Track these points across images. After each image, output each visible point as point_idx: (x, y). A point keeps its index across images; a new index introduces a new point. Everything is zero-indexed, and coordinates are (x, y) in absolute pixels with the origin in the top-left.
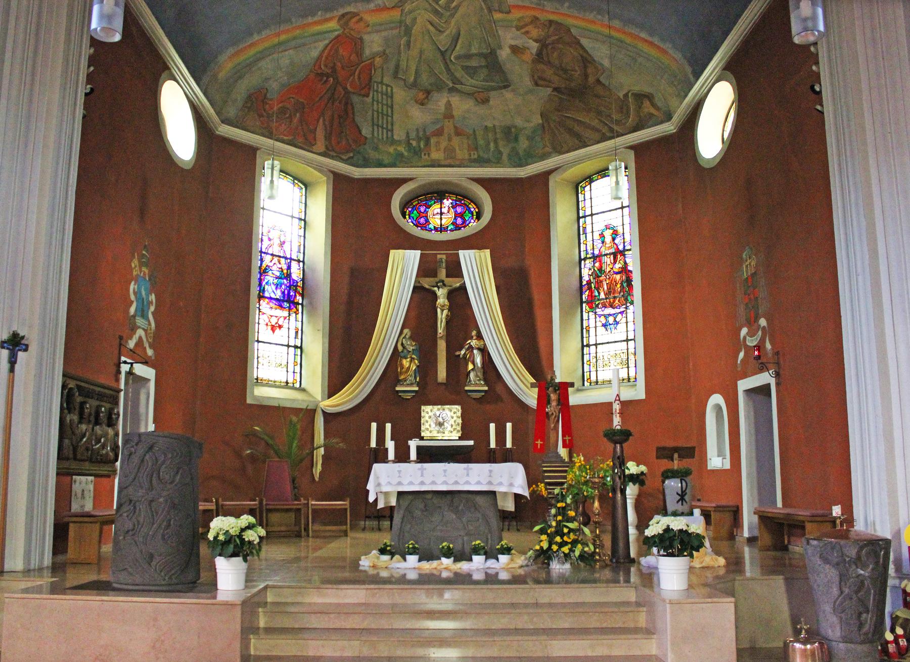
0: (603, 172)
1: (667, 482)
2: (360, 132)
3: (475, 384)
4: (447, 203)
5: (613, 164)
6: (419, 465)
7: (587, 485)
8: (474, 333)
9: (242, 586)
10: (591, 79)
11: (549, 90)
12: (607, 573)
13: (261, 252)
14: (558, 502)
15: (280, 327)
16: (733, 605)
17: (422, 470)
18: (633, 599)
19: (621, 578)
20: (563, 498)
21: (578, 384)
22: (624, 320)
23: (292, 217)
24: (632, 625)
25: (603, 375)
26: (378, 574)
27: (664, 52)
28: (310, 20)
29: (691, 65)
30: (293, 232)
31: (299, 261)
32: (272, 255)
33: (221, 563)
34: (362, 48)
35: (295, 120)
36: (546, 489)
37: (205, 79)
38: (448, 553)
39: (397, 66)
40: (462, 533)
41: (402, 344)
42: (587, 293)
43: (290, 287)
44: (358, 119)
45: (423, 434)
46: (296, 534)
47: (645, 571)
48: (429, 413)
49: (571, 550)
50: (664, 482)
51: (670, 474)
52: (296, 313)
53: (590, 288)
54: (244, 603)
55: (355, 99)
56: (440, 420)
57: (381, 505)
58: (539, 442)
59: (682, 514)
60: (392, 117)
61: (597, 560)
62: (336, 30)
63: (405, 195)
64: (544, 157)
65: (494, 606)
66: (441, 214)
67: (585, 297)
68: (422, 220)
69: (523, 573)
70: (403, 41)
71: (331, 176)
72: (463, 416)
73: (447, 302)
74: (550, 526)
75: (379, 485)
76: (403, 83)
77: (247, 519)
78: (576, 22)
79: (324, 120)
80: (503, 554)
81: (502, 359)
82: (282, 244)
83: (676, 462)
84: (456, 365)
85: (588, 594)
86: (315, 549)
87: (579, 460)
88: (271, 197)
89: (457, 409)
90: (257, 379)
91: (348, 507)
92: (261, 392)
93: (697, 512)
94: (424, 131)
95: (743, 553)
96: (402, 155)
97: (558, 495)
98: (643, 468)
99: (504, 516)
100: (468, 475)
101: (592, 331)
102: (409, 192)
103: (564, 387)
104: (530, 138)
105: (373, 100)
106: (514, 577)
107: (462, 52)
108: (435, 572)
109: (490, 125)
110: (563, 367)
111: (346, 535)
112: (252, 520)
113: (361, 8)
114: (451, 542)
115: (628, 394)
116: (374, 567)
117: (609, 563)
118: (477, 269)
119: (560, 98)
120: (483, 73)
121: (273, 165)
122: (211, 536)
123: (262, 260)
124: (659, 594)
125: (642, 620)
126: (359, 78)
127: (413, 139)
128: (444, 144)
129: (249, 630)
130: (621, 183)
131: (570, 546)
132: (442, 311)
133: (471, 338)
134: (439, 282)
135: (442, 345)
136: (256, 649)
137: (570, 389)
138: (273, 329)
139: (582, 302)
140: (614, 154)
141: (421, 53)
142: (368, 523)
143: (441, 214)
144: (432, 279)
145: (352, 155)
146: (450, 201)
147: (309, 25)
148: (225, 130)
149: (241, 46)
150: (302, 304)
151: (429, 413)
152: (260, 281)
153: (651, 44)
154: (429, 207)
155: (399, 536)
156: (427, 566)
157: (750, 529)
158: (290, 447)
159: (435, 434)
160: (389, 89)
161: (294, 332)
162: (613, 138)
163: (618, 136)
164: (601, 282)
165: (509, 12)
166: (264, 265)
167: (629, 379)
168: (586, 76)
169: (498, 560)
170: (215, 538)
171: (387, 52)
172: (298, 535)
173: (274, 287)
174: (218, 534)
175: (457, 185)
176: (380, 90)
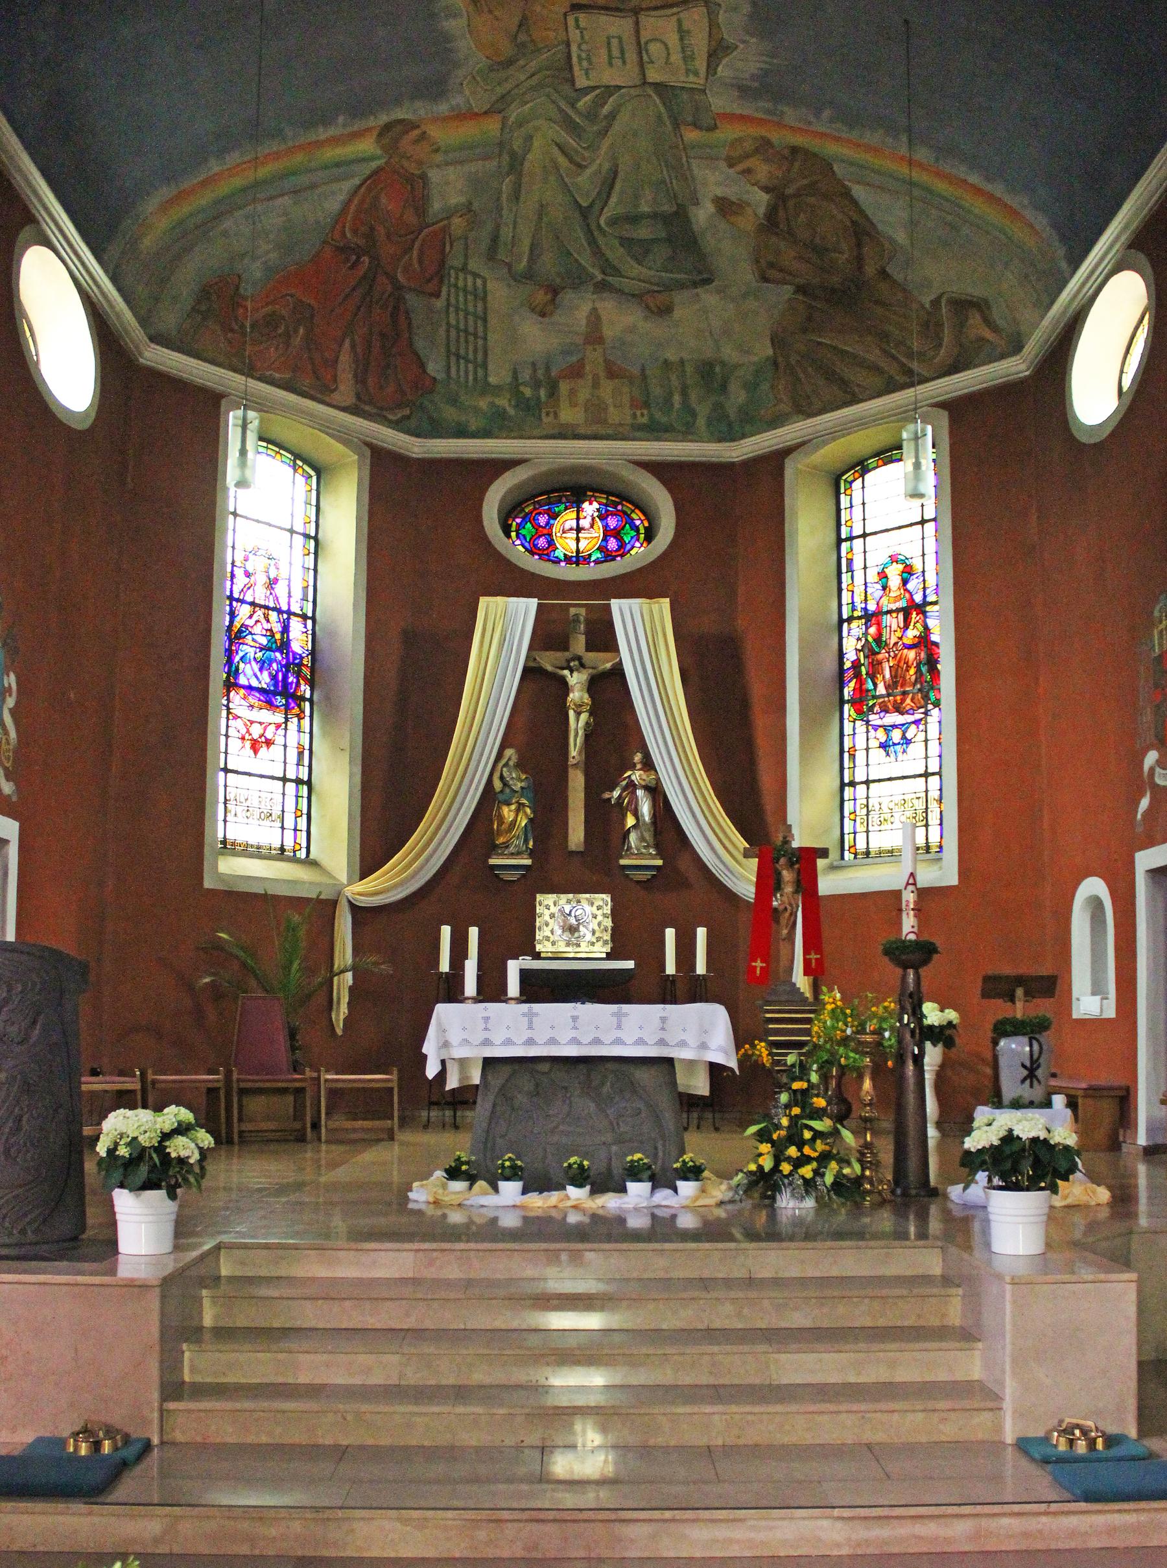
0: (889, 453)
1: (1002, 1043)
2: (422, 366)
3: (639, 854)
4: (590, 509)
5: (911, 427)
6: (525, 1007)
7: (846, 1046)
8: (638, 757)
9: (167, 1246)
10: (870, 270)
11: (789, 288)
12: (885, 1220)
13: (231, 598)
14: (794, 1079)
15: (269, 743)
16: (1134, 1286)
17: (531, 1015)
18: (937, 1271)
19: (912, 1229)
20: (804, 1069)
21: (834, 854)
22: (921, 736)
23: (292, 531)
24: (935, 1322)
25: (880, 841)
26: (444, 1216)
27: (1014, 213)
28: (322, 134)
29: (1063, 238)
30: (292, 564)
31: (304, 617)
32: (253, 604)
33: (125, 1202)
34: (426, 199)
35: (297, 341)
36: (770, 1054)
37: (114, 251)
38: (579, 1178)
39: (495, 239)
40: (608, 1137)
41: (502, 778)
42: (852, 684)
43: (287, 666)
44: (420, 344)
45: (539, 948)
46: (297, 1134)
47: (957, 1213)
48: (551, 908)
49: (816, 1172)
50: (995, 1043)
51: (1009, 1028)
52: (300, 718)
53: (858, 675)
54: (167, 1282)
55: (412, 300)
56: (573, 921)
57: (452, 1083)
58: (759, 964)
59: (1031, 1105)
60: (485, 339)
61: (869, 1192)
62: (379, 158)
63: (510, 491)
64: (775, 422)
65: (666, 1283)
66: (578, 531)
67: (847, 692)
68: (542, 542)
69: (723, 1215)
70: (507, 185)
71: (368, 453)
72: (615, 914)
73: (586, 699)
74: (778, 1127)
75: (446, 1045)
76: (506, 270)
77: (175, 1114)
78: (840, 149)
79: (353, 346)
80: (686, 1179)
81: (694, 816)
82: (272, 583)
83: (1019, 1005)
84: (604, 820)
85: (850, 1261)
86: (333, 1165)
87: (833, 998)
88: (242, 484)
89: (604, 901)
90: (224, 842)
91: (395, 1085)
92: (231, 867)
93: (1059, 1100)
94: (548, 369)
95: (1135, 1176)
96: (501, 414)
97: (793, 1066)
98: (951, 1015)
99: (689, 1102)
100: (619, 1027)
101: (860, 757)
102: (519, 487)
103: (807, 859)
104: (751, 387)
105: (448, 305)
106: (706, 1223)
107: (620, 210)
108: (554, 1213)
109: (671, 355)
110: (805, 819)
111: (392, 1138)
112: (186, 1115)
113: (422, 112)
114: (585, 1156)
115: (929, 876)
116: (436, 1203)
117: (888, 1196)
118: (645, 635)
119: (810, 307)
120: (661, 253)
121: (244, 419)
122: (102, 1149)
123: (233, 615)
124: (989, 1262)
125: (955, 1312)
126: (420, 262)
127: (525, 384)
128: (584, 394)
129: (180, 1330)
130: (923, 468)
131: (815, 1165)
132: (578, 714)
133: (633, 767)
134: (573, 659)
135: (577, 782)
136: (193, 1370)
137: (821, 863)
138: (255, 746)
139: (842, 702)
140: (907, 415)
141: (542, 208)
142: (434, 1113)
143: (579, 529)
144: (559, 654)
145: (407, 412)
146: (596, 505)
147: (319, 144)
148: (158, 357)
149: (186, 185)
150: (311, 701)
151: (551, 908)
152: (230, 654)
153: (991, 198)
154: (555, 516)
155: (485, 1143)
156: (538, 1202)
157: (1150, 1131)
158: (287, 967)
159: (561, 947)
160: (479, 282)
161: (295, 752)
162: (912, 385)
163: (920, 382)
164: (880, 663)
165: (712, 128)
166: (237, 625)
167: (928, 848)
168: (859, 260)
169: (675, 1190)
170: (111, 1152)
171: (476, 206)
172: (301, 1139)
173: (256, 667)
174: (116, 1144)
175: (613, 476)
176: (461, 284)
